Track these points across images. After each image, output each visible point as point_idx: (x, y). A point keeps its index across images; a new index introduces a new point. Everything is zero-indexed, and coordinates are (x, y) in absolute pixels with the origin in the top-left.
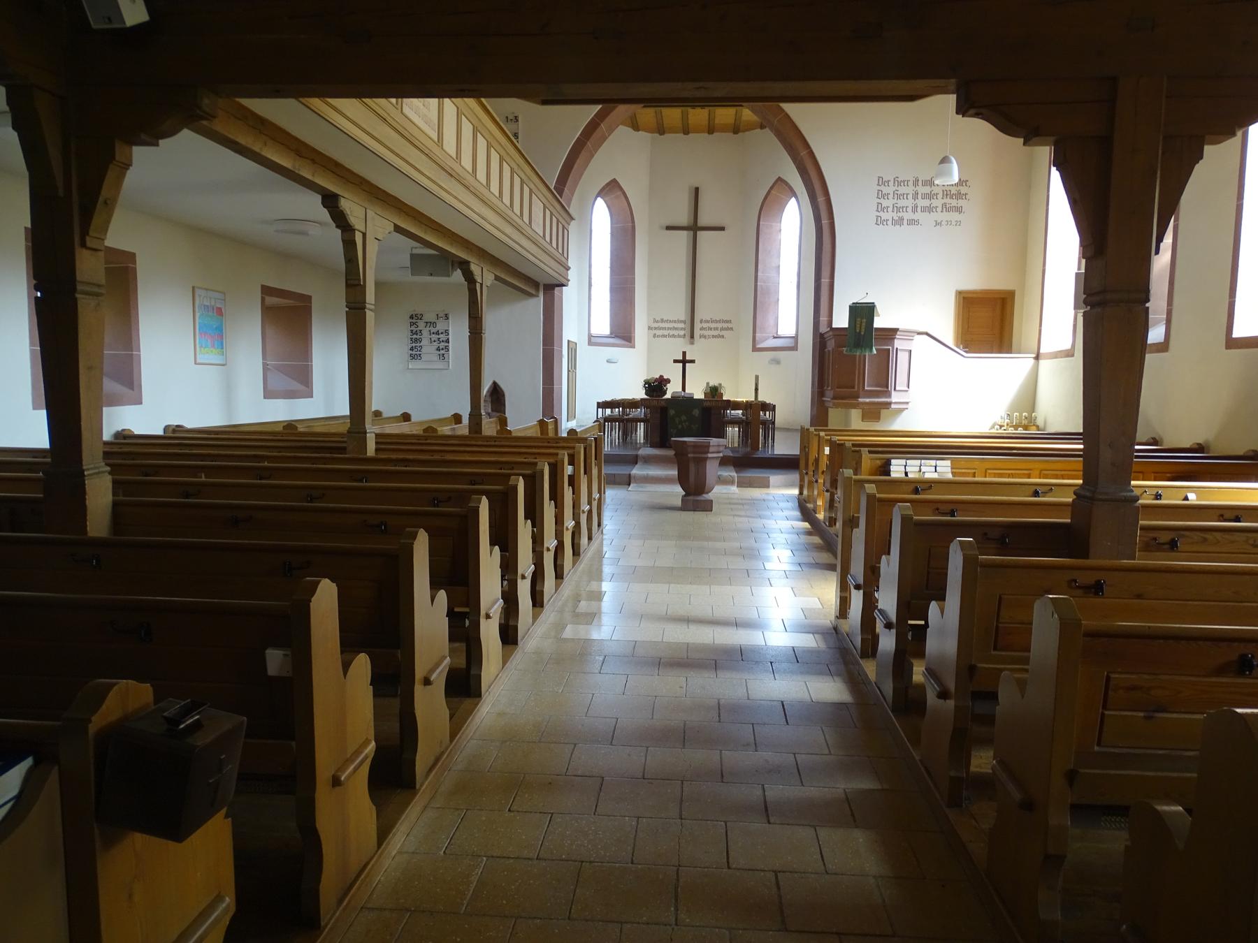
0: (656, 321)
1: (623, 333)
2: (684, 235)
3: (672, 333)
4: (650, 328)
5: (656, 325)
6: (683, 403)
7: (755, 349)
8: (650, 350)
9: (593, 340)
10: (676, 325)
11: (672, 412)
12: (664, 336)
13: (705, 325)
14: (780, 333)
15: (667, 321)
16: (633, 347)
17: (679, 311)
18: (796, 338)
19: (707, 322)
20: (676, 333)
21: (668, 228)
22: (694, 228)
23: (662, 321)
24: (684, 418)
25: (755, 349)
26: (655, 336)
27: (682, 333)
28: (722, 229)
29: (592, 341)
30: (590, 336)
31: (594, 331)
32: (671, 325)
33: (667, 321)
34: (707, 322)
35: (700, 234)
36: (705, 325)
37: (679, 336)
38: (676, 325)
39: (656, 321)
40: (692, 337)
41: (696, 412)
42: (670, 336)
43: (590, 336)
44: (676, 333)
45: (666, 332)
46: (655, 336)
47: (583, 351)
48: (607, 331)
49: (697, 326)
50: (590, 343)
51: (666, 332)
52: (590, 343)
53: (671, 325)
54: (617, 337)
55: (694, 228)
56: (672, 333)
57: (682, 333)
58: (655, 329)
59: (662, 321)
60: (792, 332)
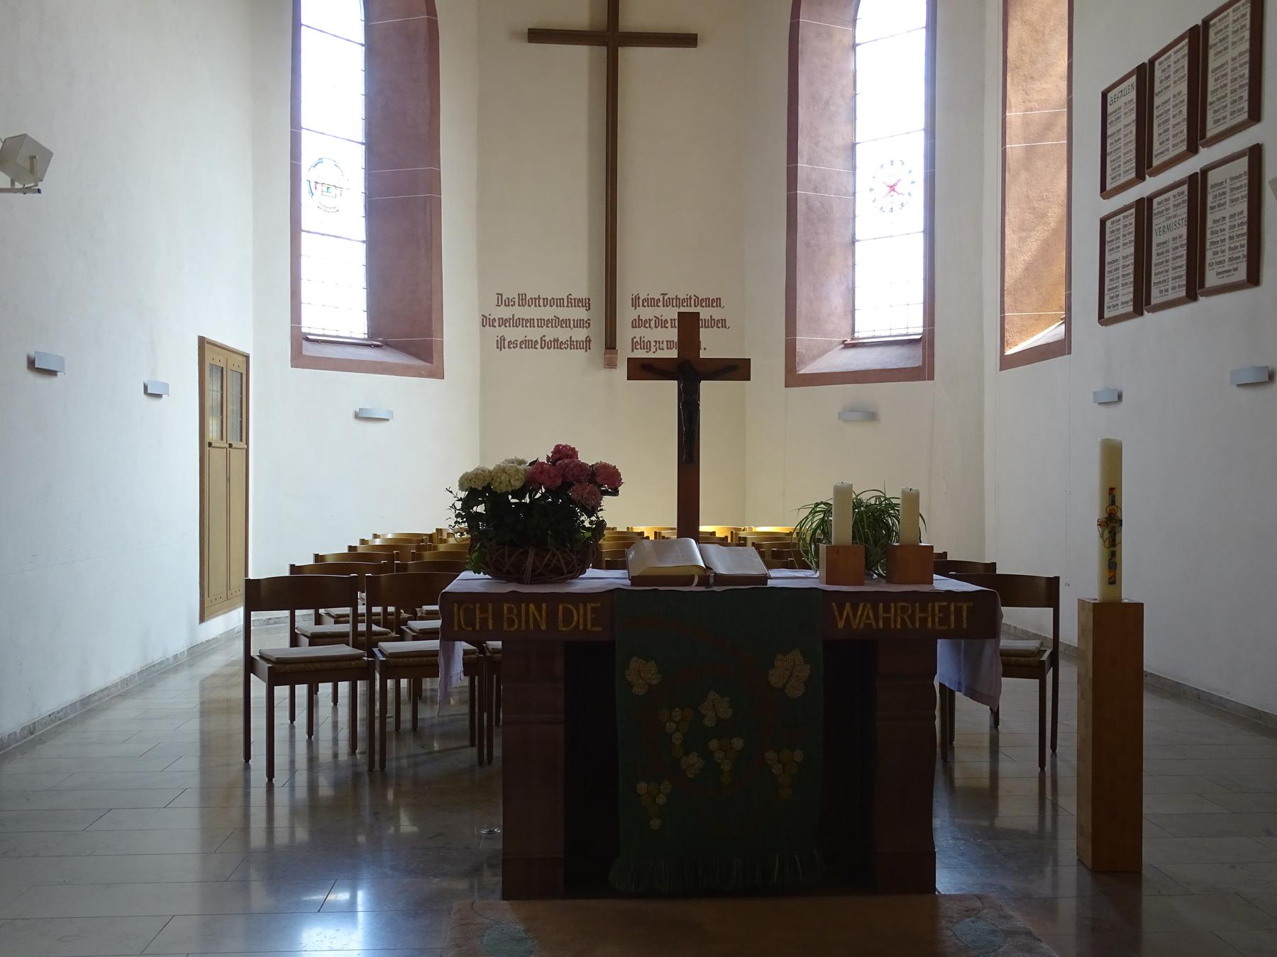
0: (502, 301)
1: (404, 329)
2: (581, 57)
3: (551, 333)
4: (486, 321)
5: (505, 312)
6: (704, 619)
7: (793, 378)
8: (488, 383)
9: (309, 350)
10: (564, 313)
11: (641, 674)
12: (528, 344)
13: (646, 313)
14: (864, 330)
15: (536, 301)
16: (439, 374)
17: (573, 273)
18: (926, 342)
19: (652, 303)
20: (563, 334)
21: (538, 35)
22: (610, 37)
23: (523, 300)
24: (717, 707)
25: (793, 378)
26: (501, 343)
27: (580, 334)
28: (689, 40)
29: (306, 351)
30: (299, 339)
31: (312, 323)
32: (548, 313)
33: (536, 301)
34: (652, 303)
35: (631, 57)
36: (646, 313)
37: (572, 344)
38: (564, 313)
39: (502, 301)
40: (611, 345)
41: (791, 672)
42: (545, 344)
43: (299, 339)
44: (563, 334)
45: (534, 334)
46: (501, 343)
47: (275, 389)
48: (357, 326)
49: (626, 315)
50: (299, 359)
51: (534, 334)
52: (299, 359)
53: (548, 313)
54: (386, 345)
55: (610, 37)
56: (551, 333)
57: (580, 334)
58: (506, 323)
59: (523, 300)
60: (913, 324)
